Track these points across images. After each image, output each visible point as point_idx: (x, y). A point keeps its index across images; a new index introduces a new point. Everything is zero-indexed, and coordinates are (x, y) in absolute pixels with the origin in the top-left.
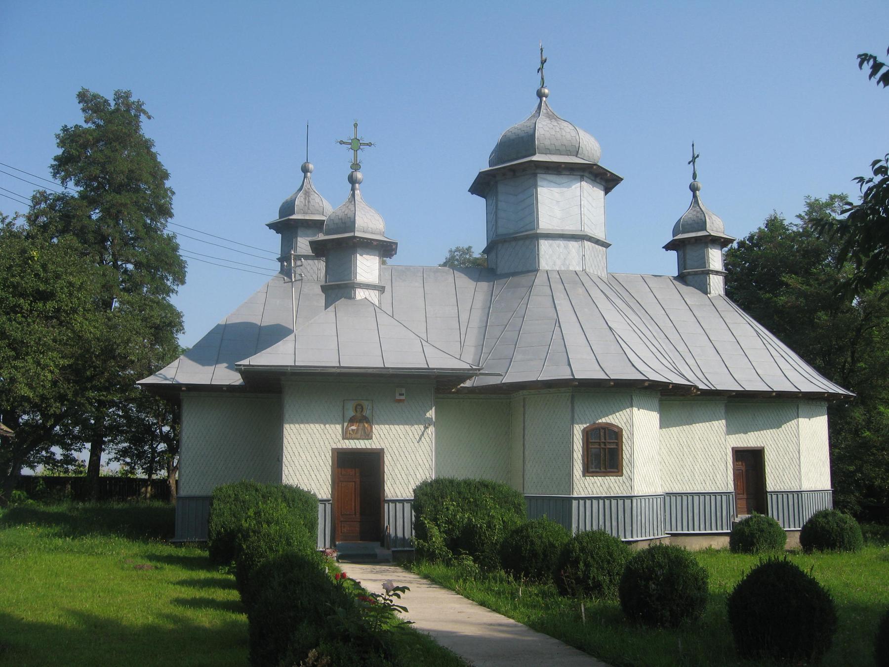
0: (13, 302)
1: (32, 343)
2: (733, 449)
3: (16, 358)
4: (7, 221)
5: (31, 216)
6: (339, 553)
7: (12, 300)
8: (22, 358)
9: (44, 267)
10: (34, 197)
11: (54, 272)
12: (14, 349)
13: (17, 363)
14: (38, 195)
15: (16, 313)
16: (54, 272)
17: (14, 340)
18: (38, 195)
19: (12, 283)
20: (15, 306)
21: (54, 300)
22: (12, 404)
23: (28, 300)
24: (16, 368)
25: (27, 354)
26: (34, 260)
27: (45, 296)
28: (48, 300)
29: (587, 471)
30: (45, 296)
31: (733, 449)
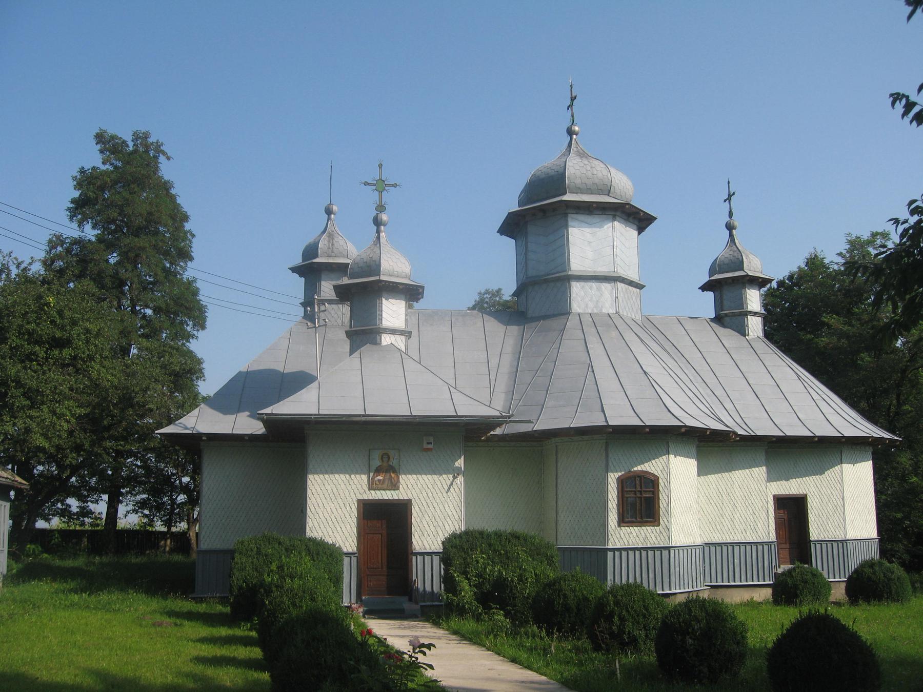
3: (31, 407)
4: (23, 266)
7: (28, 348)
9: (60, 313)
10: (50, 241)
11: (70, 318)
12: (29, 398)
13: (33, 413)
14: (54, 239)
15: (31, 361)
16: (70, 318)
18: (54, 239)
20: (30, 354)
23: (43, 347)
25: (43, 403)
27: (61, 344)
28: (65, 347)
30: (61, 344)
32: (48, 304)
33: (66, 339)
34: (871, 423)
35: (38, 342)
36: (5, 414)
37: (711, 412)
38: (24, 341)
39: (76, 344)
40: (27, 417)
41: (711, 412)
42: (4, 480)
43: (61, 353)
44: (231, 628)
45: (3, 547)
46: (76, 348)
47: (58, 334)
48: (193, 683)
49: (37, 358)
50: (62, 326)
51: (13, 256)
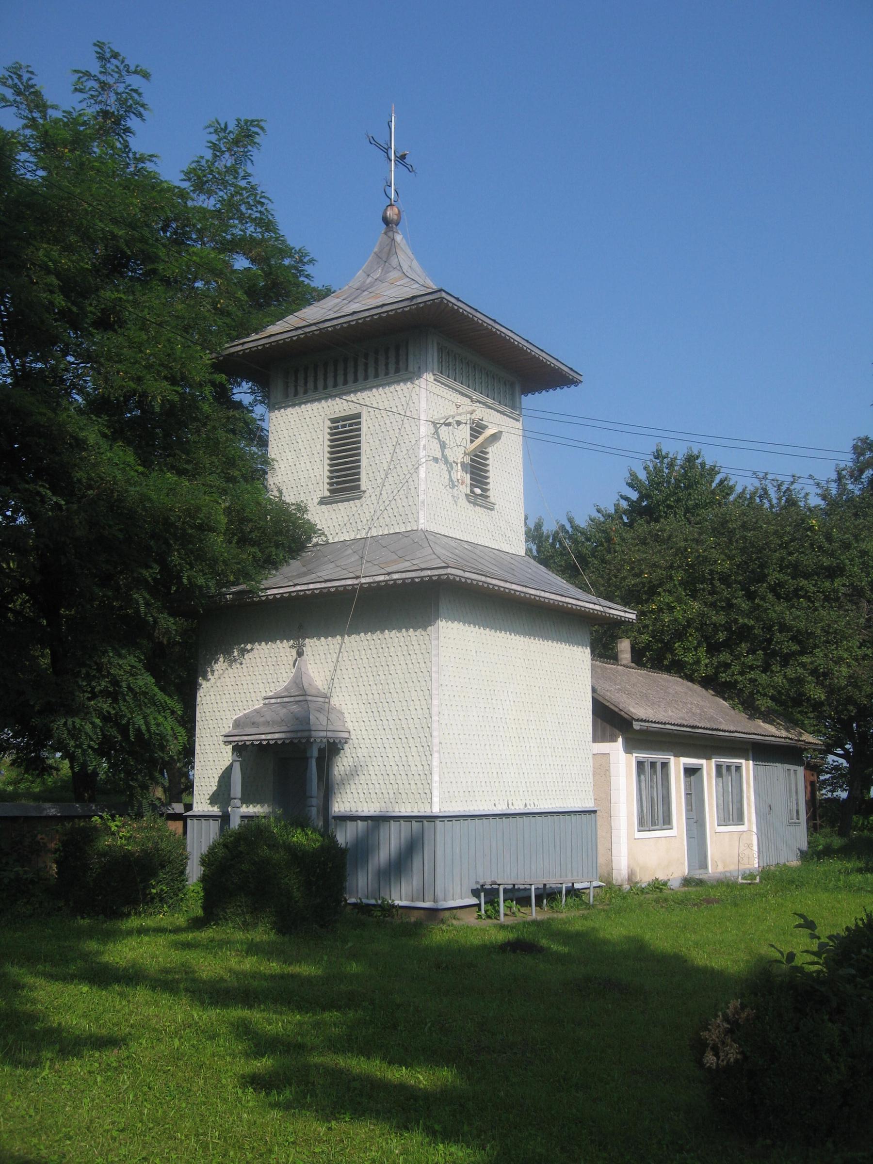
0: (793, 586)
1: (819, 631)
2: (595, 740)
3: (802, 653)
4: (784, 488)
5: (853, 471)
6: (425, 942)
7: (792, 584)
8: (811, 652)
9: (829, 538)
10: (855, 447)
11: (841, 541)
12: (799, 643)
13: (805, 659)
14: (859, 444)
15: (799, 597)
16: (841, 541)
17: (798, 631)
18: (859, 444)
19: (790, 563)
20: (796, 590)
21: (844, 575)
22: (836, 708)
23: (812, 580)
24: (803, 665)
25: (816, 646)
26: (815, 529)
27: (833, 573)
28: (836, 577)
29: (702, 765)
30: (833, 573)
31: (595, 740)
32: (811, 529)
33: (837, 567)
34: (457, 385)
35: (807, 576)
36: (774, 664)
37: (720, 730)
38: (789, 575)
39: (850, 571)
40: (799, 664)
41: (720, 730)
42: (783, 740)
43: (833, 584)
44: (105, 988)
45: (798, 819)
46: (850, 575)
47: (826, 562)
48: (134, 1046)
49: (806, 594)
50: (832, 551)
51: (770, 477)
